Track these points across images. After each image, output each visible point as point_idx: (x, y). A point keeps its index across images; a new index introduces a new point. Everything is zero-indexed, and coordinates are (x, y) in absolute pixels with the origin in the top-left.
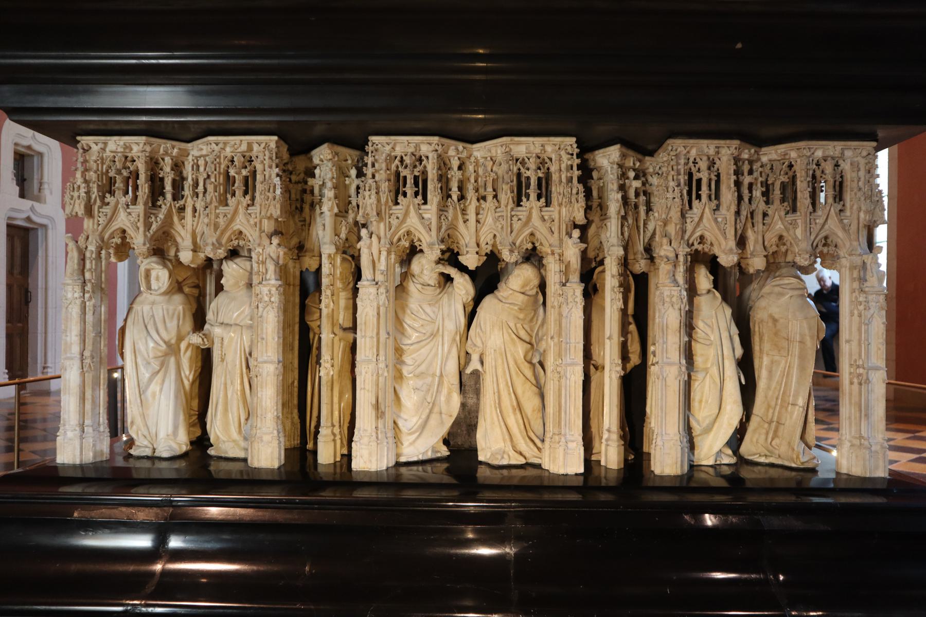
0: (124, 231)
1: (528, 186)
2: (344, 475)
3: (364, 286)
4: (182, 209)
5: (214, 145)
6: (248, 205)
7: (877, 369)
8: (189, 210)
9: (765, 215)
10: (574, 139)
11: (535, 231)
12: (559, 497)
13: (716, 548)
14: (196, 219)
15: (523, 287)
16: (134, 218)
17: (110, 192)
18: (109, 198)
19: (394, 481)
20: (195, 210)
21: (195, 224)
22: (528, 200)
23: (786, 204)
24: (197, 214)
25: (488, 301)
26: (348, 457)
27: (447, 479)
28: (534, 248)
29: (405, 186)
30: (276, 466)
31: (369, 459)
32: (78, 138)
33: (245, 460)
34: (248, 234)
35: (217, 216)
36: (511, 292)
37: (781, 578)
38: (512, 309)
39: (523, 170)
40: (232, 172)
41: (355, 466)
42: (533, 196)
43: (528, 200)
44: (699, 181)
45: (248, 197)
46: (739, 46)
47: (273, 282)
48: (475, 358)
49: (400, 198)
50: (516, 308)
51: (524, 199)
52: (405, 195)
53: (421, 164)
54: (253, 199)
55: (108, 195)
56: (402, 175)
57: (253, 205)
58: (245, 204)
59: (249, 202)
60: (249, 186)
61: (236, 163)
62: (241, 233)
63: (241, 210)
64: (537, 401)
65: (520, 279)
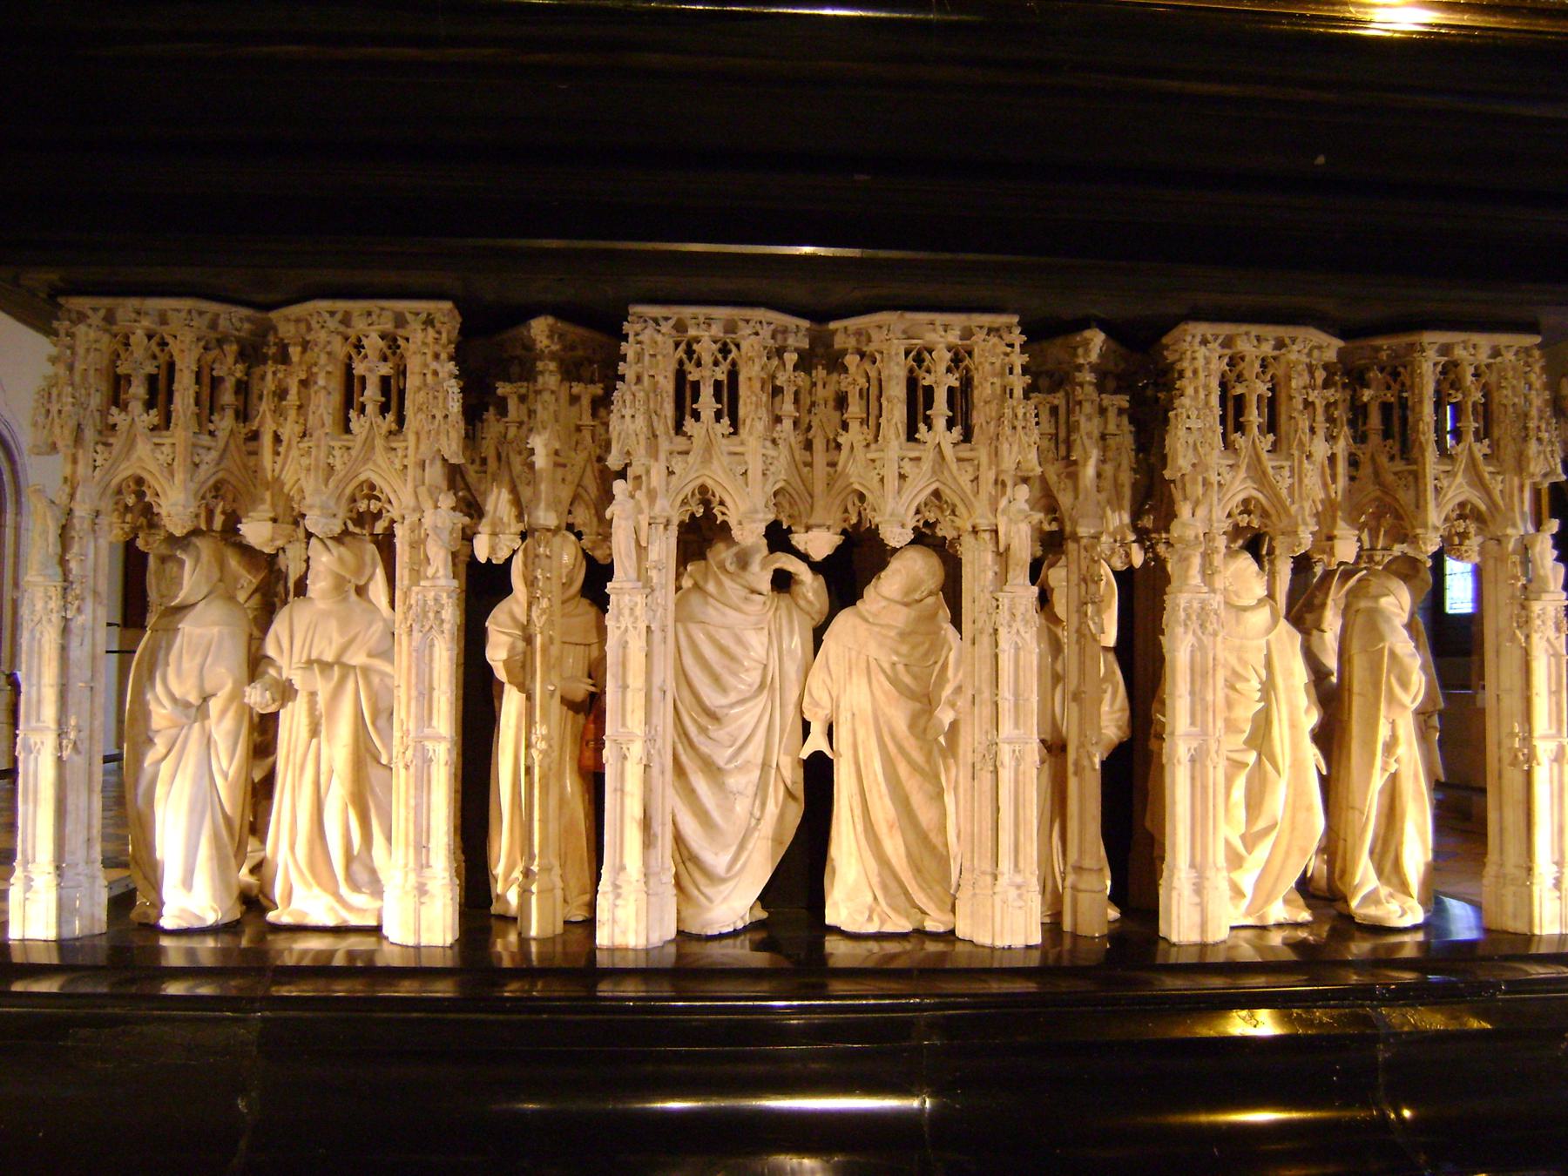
0: (140, 481)
1: (929, 403)
2: (577, 960)
3: (621, 591)
4: (255, 436)
5: (327, 316)
6: (390, 432)
7: (1544, 737)
8: (267, 439)
9: (277, 439)
10: (1016, 319)
11: (942, 488)
12: (995, 987)
13: (1252, 1072)
14: (280, 460)
15: (907, 594)
16: (163, 456)
17: (117, 405)
18: (116, 416)
19: (687, 963)
20: (277, 439)
21: (278, 467)
22: (930, 428)
23: (153, 412)
24: (282, 449)
25: (844, 618)
26: (590, 924)
27: (761, 959)
28: (709, 515)
29: (695, 399)
30: (449, 940)
31: (630, 922)
32: (62, 300)
33: (376, 931)
34: (387, 489)
35: (330, 454)
36: (884, 603)
37: (1407, 1113)
38: (885, 636)
39: (689, 367)
40: (359, 368)
41: (603, 938)
42: (940, 423)
43: (930, 428)
44: (929, 391)
45: (390, 417)
46: (1321, 160)
47: (442, 582)
48: (817, 729)
49: (689, 423)
50: (892, 633)
51: (922, 427)
52: (696, 415)
53: (725, 358)
54: (401, 420)
55: (114, 410)
56: (690, 378)
57: (167, 428)
58: (384, 431)
59: (394, 427)
60: (393, 398)
61: (368, 351)
62: (372, 487)
63: (379, 443)
64: (679, 819)
65: (906, 575)
